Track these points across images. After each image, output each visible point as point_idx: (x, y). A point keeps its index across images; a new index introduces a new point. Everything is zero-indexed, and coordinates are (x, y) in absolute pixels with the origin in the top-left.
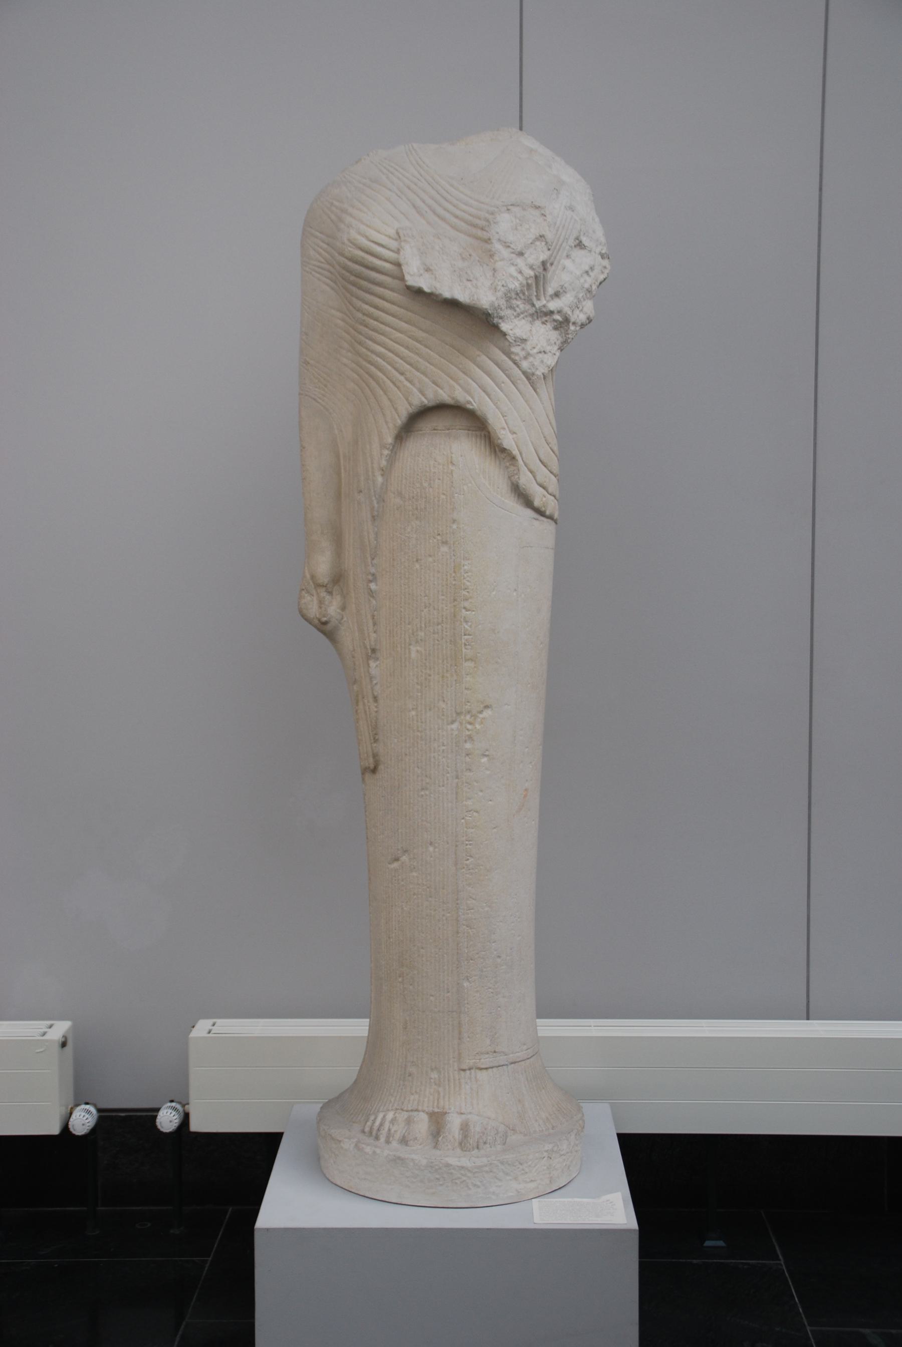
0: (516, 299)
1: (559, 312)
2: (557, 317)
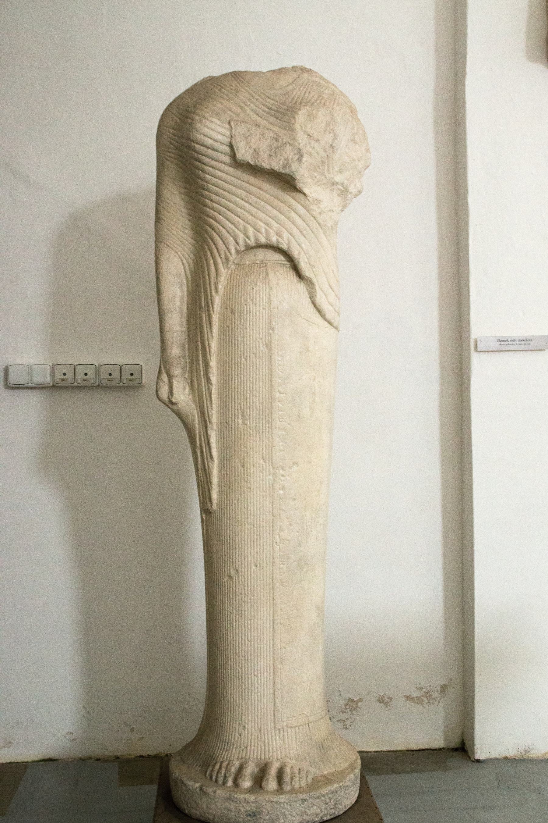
1: (342, 184)
2: (340, 187)
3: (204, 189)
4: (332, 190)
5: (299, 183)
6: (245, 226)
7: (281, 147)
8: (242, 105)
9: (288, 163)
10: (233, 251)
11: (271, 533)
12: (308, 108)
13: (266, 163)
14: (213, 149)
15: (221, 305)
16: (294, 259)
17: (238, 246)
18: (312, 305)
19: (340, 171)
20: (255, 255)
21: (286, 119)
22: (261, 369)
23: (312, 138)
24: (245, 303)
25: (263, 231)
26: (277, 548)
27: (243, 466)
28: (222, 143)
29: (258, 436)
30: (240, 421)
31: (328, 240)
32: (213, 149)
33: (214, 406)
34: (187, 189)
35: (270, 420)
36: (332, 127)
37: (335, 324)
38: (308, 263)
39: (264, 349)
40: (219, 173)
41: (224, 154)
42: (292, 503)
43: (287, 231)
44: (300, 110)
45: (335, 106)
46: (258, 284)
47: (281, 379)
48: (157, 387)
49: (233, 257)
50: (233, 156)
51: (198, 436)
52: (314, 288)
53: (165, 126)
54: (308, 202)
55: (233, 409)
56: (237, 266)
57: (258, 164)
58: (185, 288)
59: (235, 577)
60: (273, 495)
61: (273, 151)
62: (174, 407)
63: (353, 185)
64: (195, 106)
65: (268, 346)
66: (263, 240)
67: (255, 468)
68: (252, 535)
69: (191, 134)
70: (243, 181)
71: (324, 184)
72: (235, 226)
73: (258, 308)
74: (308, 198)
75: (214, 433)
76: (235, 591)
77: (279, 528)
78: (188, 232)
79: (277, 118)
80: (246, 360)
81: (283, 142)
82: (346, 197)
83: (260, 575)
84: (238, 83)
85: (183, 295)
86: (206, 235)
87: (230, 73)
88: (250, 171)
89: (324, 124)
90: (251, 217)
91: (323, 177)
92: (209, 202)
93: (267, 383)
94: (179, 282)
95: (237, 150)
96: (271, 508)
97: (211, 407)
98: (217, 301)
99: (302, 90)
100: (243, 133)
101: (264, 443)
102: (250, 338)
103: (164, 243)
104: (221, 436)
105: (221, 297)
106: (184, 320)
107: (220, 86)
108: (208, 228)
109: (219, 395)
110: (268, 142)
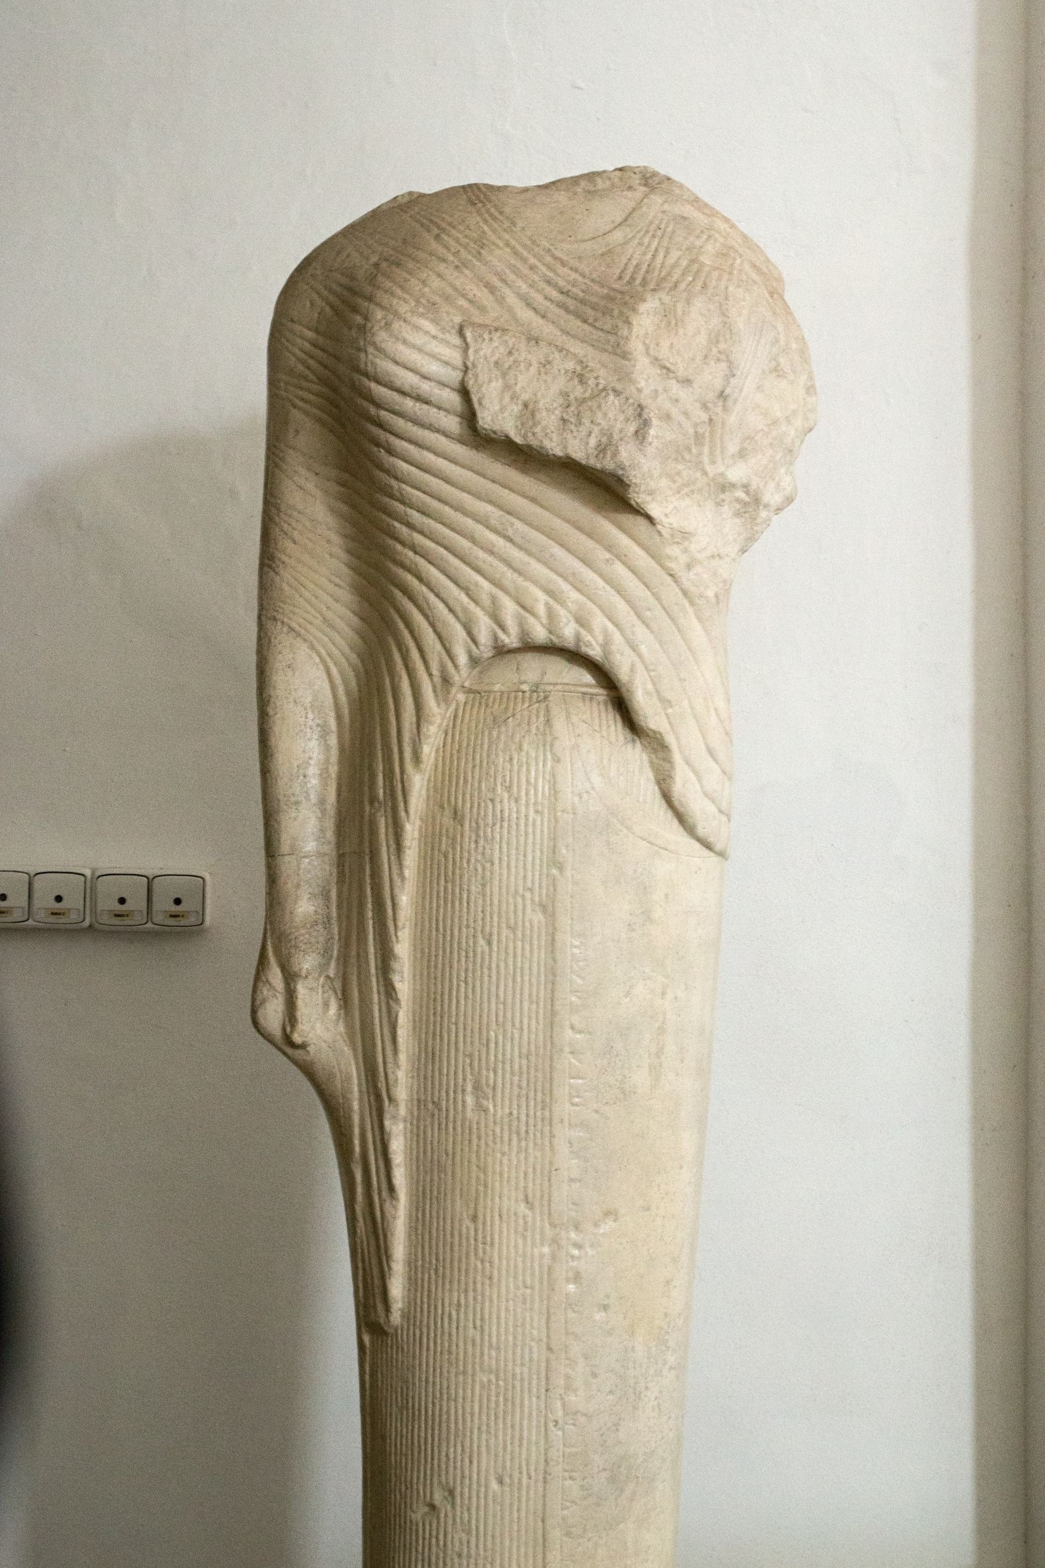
0: (676, 459)
1: (746, 487)
2: (740, 494)
3: (392, 496)
4: (718, 504)
5: (637, 493)
6: (494, 599)
7: (593, 397)
8: (495, 281)
9: (610, 443)
10: (463, 659)
11: (543, 1397)
12: (663, 295)
13: (555, 439)
14: (419, 398)
15: (428, 797)
16: (618, 685)
17: (473, 647)
18: (663, 802)
19: (742, 454)
20: (517, 669)
21: (607, 323)
22: (527, 966)
23: (671, 375)
24: (490, 795)
25: (541, 610)
26: (556, 1434)
27: (474, 1218)
28: (443, 384)
29: (515, 1142)
30: (470, 1100)
31: (707, 632)
32: (419, 398)
33: (403, 1057)
34: (343, 485)
35: (548, 1100)
36: (722, 346)
37: (718, 847)
38: (655, 694)
39: (538, 918)
40: (429, 458)
41: (446, 410)
42: (599, 1316)
43: (603, 611)
44: (644, 301)
45: (731, 289)
46: (525, 747)
47: (579, 994)
48: (254, 1000)
49: (463, 675)
50: (470, 416)
51: (356, 1131)
52: (668, 760)
53: (292, 321)
54: (657, 538)
55: (453, 1069)
56: (472, 696)
57: (534, 443)
58: (333, 741)
59: (444, 1508)
60: (549, 1297)
61: (572, 408)
62: (298, 1054)
63: (771, 485)
64: (372, 280)
65: (548, 908)
66: (540, 634)
67: (505, 1225)
68: (493, 1398)
69: (362, 355)
70: (493, 481)
71: (700, 490)
72: (468, 595)
73: (523, 809)
74: (659, 527)
75: (401, 1126)
76: (445, 1545)
77: (562, 1382)
78: (346, 595)
79: (585, 321)
80: (489, 943)
81: (597, 385)
82: (755, 519)
83: (511, 1504)
84: (485, 221)
85: (327, 760)
86: (392, 611)
87: (463, 187)
88: (513, 457)
89: (702, 339)
90: (509, 574)
91: (698, 474)
92: (403, 531)
93: (542, 1004)
94: (318, 725)
95: (480, 404)
96: (544, 1330)
97: (395, 1060)
98: (419, 784)
99: (649, 244)
100: (495, 358)
101: (531, 1159)
102: (500, 888)
103: (283, 623)
104: (418, 1136)
105: (427, 776)
106: (330, 824)
107: (438, 227)
108: (398, 594)
109: (419, 1024)
110: (561, 383)
